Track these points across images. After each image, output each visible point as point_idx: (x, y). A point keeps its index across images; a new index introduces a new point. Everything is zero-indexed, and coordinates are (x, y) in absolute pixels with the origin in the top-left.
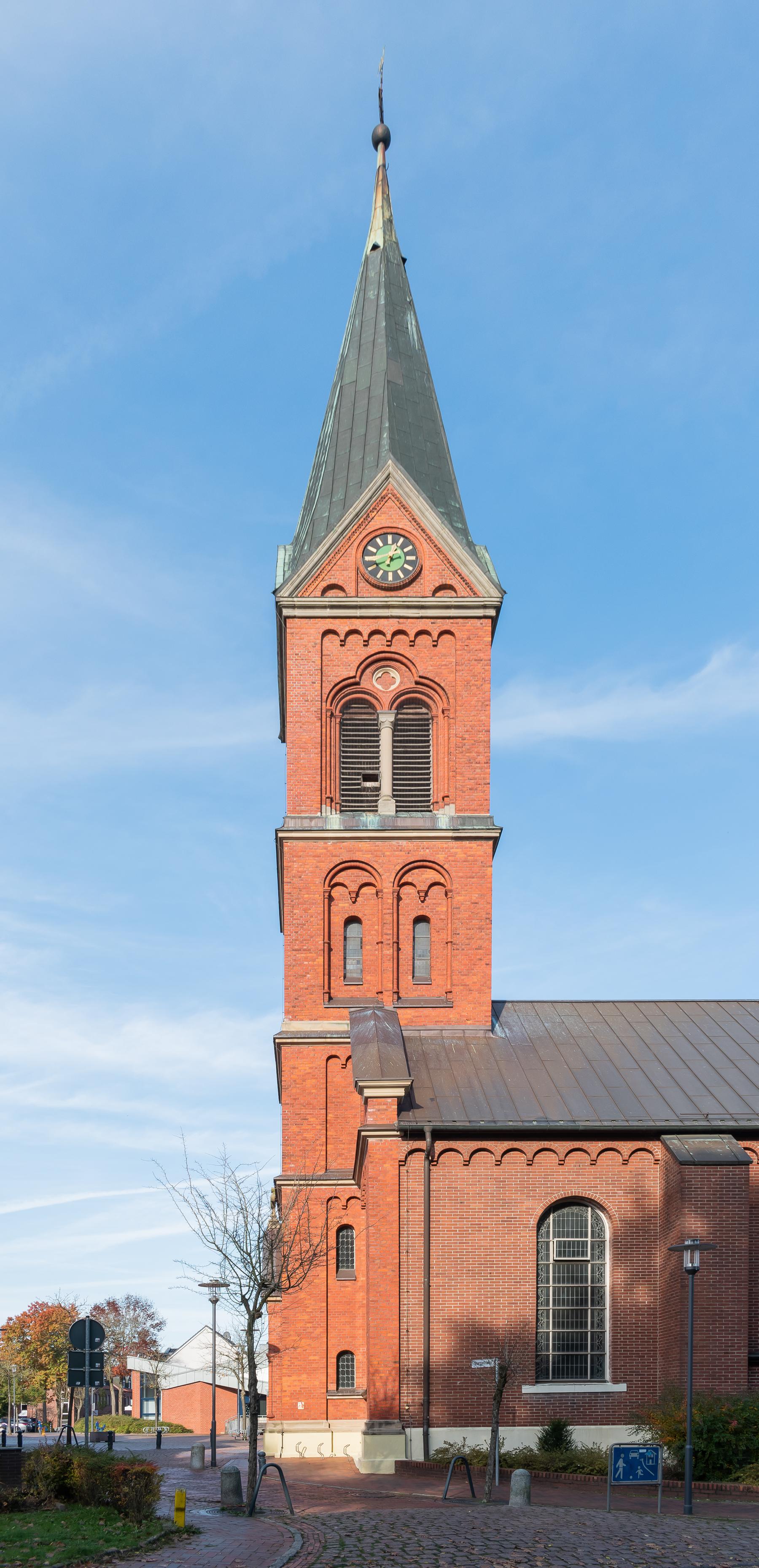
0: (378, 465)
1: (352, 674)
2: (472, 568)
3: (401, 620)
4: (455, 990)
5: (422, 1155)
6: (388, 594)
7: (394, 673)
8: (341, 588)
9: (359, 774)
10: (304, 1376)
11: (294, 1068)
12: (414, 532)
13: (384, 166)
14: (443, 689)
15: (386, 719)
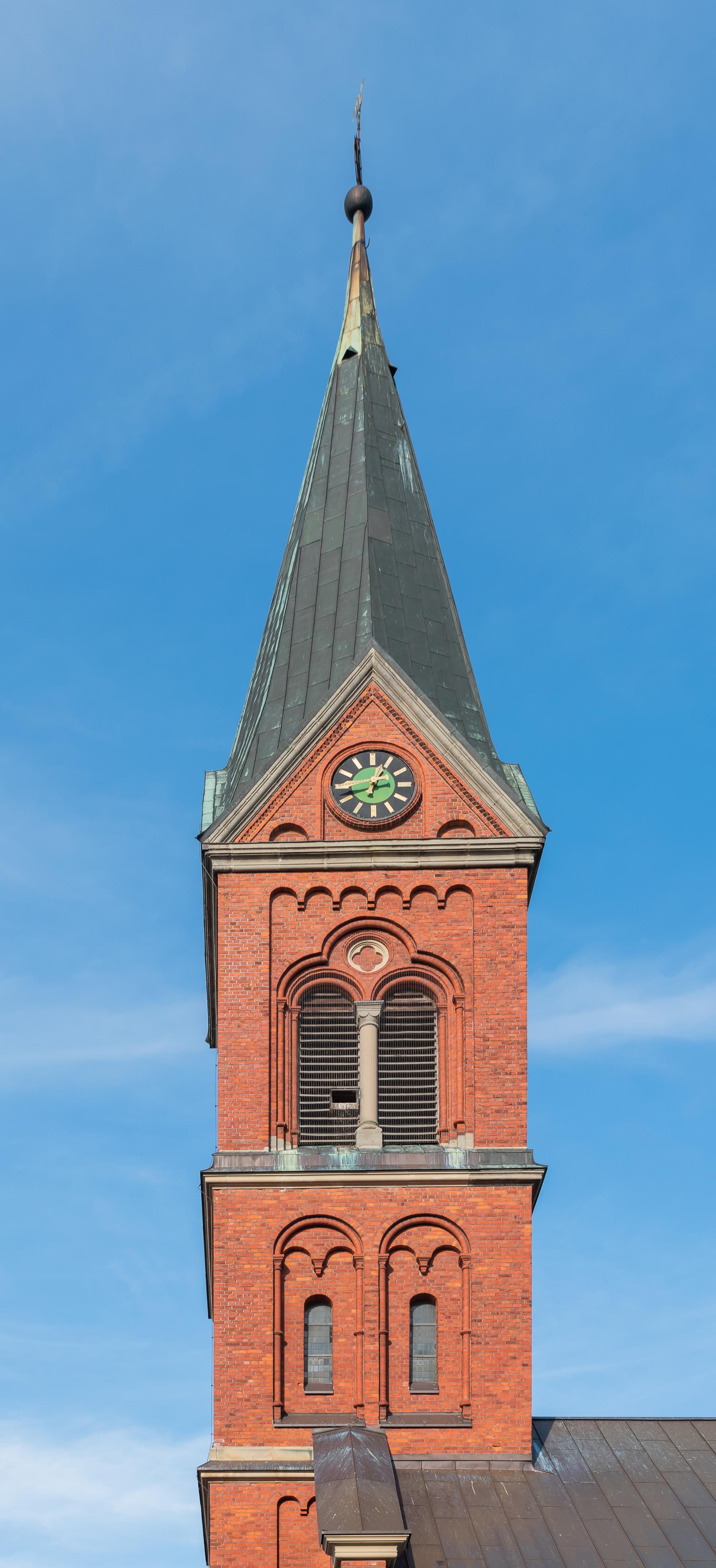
0: (354, 656)
1: (316, 949)
2: (497, 797)
3: (390, 873)
4: (476, 1402)
9: (327, 1091)
11: (229, 1515)
12: (410, 748)
13: (363, 242)
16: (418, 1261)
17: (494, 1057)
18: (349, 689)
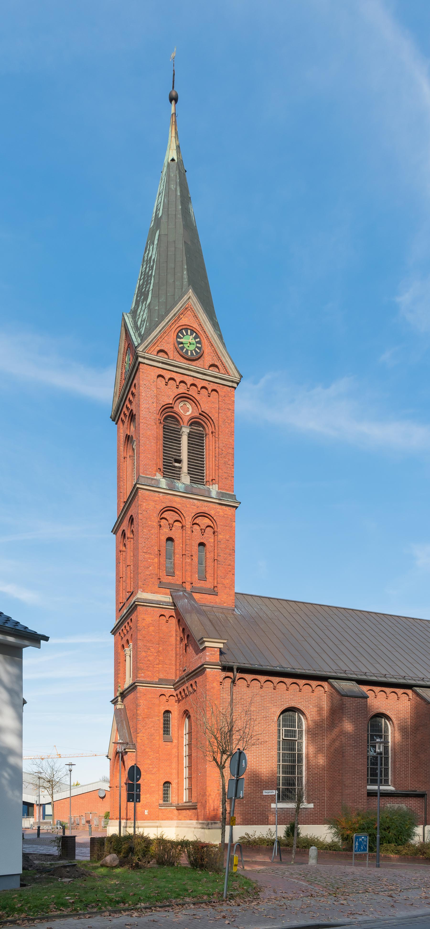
0: (186, 292)
1: (171, 402)
2: (227, 359)
3: (194, 379)
4: (219, 586)
5: (230, 680)
6: (190, 362)
7: (188, 406)
8: (166, 353)
9: (173, 458)
10: (148, 795)
11: (144, 619)
12: (200, 331)
14: (213, 421)
15: (186, 430)
16: (201, 530)
17: (225, 457)
18: (183, 303)
